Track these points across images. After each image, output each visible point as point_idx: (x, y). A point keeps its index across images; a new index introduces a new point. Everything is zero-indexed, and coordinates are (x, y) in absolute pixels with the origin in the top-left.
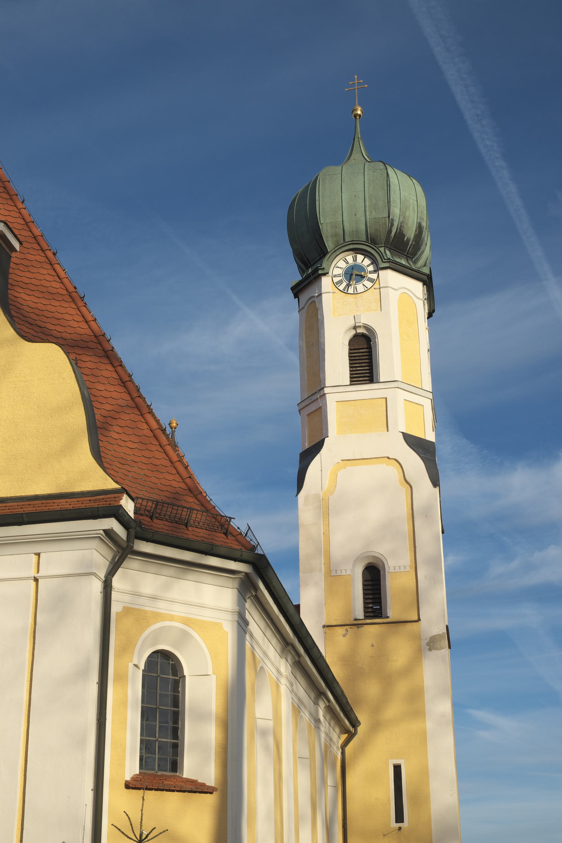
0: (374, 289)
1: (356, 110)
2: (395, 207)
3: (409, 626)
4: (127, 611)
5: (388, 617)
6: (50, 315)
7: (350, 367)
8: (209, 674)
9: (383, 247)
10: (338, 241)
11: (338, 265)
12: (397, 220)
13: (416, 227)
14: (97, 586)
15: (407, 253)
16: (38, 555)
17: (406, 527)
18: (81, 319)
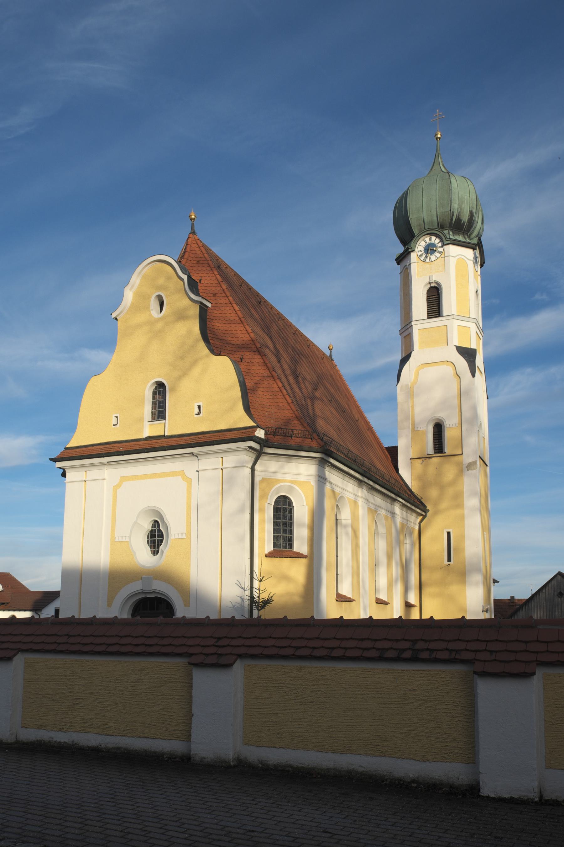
1: (437, 134)
2: (454, 203)
3: (456, 458)
4: (264, 480)
5: (445, 453)
6: (231, 332)
7: (428, 307)
9: (448, 229)
11: (421, 244)
13: (469, 214)
14: (248, 471)
16: (222, 458)
17: (456, 402)
18: (245, 332)
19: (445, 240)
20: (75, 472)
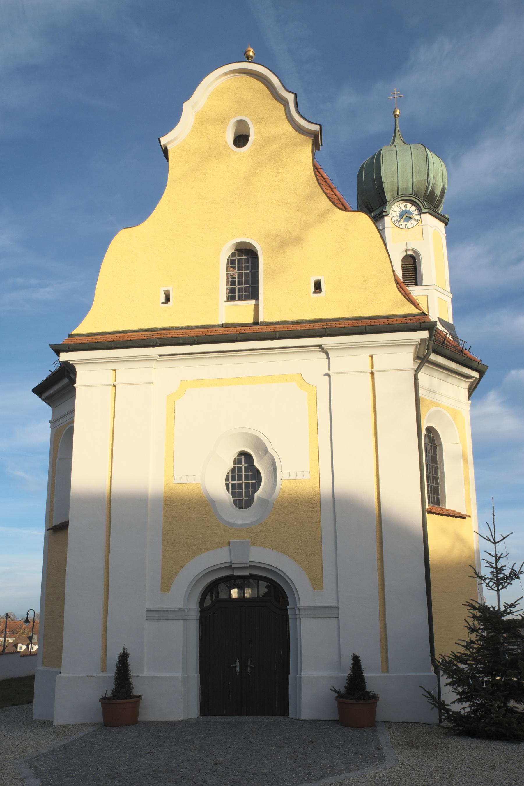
0: (419, 226)
8: (458, 443)
10: (394, 195)
11: (395, 210)
12: (432, 182)
15: (435, 205)
19: (423, 208)
20: (197, 327)
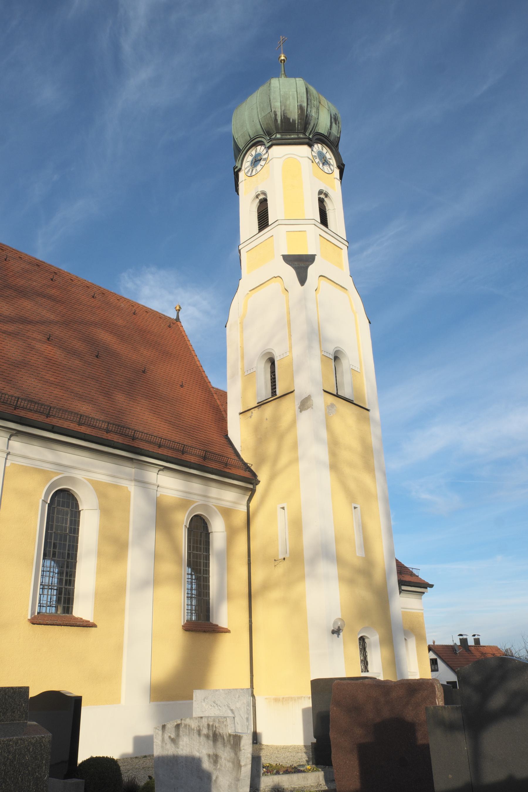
2: (275, 102)
